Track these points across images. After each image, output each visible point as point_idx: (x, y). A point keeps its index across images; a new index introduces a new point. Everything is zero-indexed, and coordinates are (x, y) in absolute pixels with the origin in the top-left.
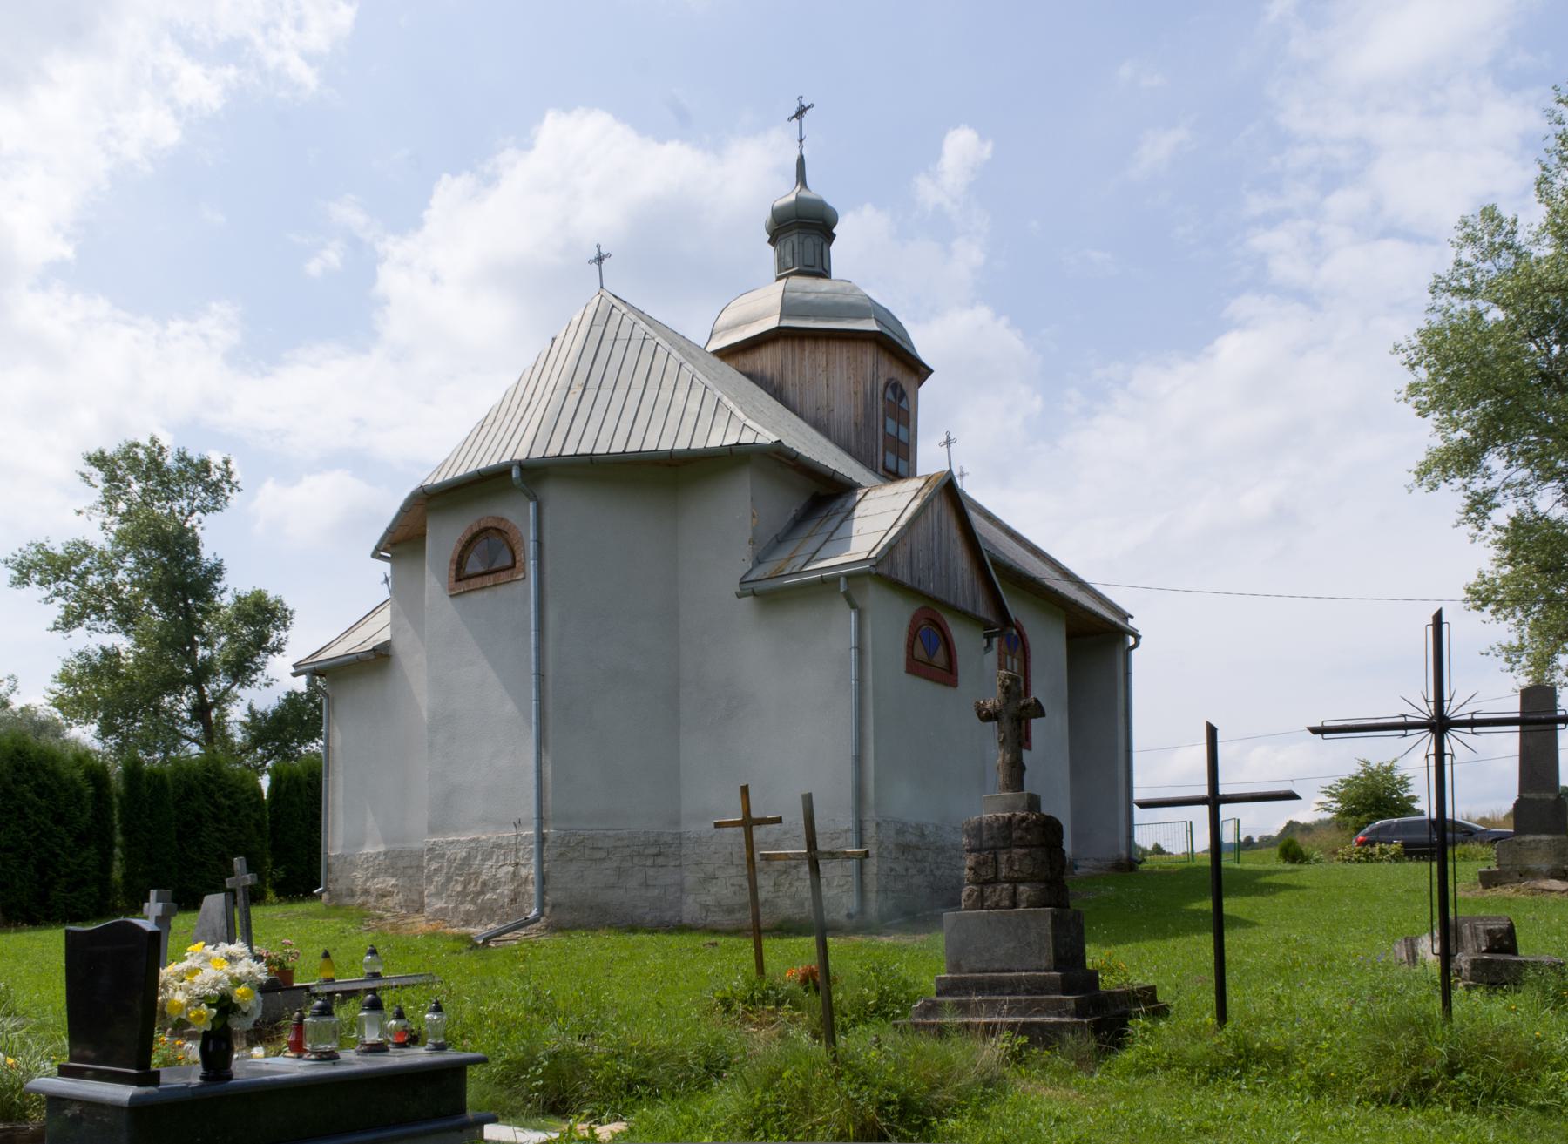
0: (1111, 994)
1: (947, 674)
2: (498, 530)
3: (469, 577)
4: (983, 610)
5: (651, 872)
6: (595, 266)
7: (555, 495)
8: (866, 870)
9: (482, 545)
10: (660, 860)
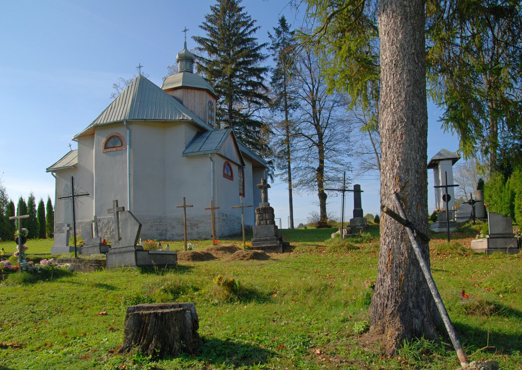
0: (203, 339)
1: (231, 178)
2: (117, 136)
3: (108, 148)
4: (239, 162)
5: (159, 226)
6: (139, 69)
7: (133, 127)
8: (215, 225)
9: (112, 140)
10: (161, 223)
